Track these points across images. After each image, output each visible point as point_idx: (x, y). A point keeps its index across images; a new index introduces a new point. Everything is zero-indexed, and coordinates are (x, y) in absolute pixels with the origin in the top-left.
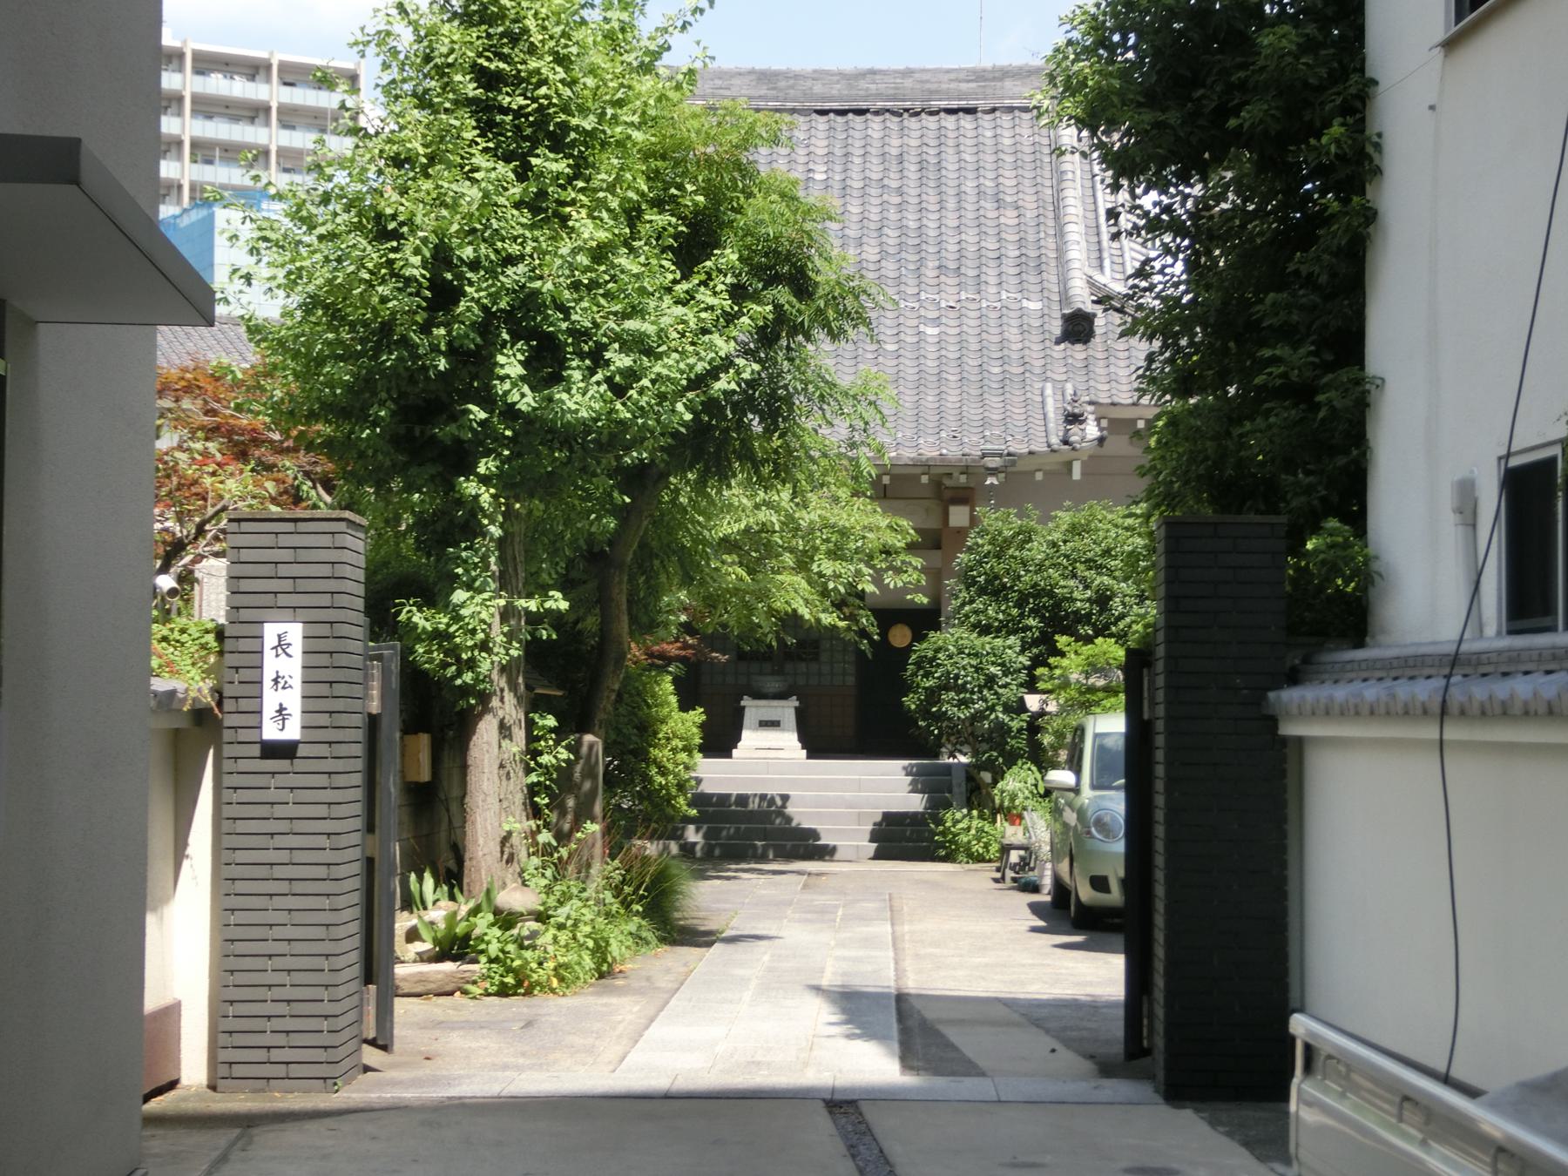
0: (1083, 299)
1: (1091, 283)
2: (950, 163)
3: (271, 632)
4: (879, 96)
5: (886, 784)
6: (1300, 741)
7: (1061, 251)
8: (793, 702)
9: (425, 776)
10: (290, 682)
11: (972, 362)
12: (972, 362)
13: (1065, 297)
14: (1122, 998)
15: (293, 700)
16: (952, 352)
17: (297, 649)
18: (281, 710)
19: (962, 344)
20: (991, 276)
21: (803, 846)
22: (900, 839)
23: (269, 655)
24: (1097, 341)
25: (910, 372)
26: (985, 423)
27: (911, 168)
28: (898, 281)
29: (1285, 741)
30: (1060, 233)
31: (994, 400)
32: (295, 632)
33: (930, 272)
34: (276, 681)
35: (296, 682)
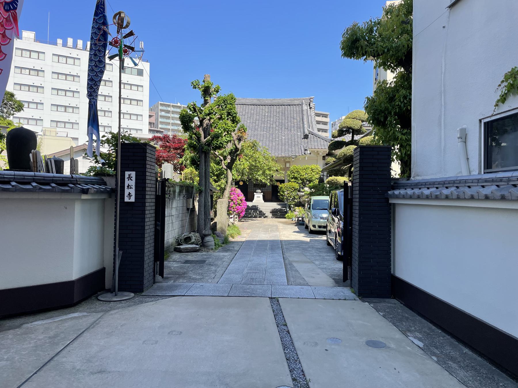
0: (307, 132)
3: (127, 173)
5: (275, 205)
6: (394, 204)
7: (303, 126)
8: (262, 194)
11: (290, 142)
12: (290, 142)
13: (304, 132)
14: (26, 40)
15: (133, 191)
17: (134, 178)
18: (129, 194)
19: (288, 139)
20: (293, 129)
21: (262, 215)
23: (126, 180)
25: (280, 144)
28: (279, 130)
29: (391, 204)
30: (303, 123)
31: (293, 148)
32: (133, 174)
34: (128, 187)
35: (134, 187)
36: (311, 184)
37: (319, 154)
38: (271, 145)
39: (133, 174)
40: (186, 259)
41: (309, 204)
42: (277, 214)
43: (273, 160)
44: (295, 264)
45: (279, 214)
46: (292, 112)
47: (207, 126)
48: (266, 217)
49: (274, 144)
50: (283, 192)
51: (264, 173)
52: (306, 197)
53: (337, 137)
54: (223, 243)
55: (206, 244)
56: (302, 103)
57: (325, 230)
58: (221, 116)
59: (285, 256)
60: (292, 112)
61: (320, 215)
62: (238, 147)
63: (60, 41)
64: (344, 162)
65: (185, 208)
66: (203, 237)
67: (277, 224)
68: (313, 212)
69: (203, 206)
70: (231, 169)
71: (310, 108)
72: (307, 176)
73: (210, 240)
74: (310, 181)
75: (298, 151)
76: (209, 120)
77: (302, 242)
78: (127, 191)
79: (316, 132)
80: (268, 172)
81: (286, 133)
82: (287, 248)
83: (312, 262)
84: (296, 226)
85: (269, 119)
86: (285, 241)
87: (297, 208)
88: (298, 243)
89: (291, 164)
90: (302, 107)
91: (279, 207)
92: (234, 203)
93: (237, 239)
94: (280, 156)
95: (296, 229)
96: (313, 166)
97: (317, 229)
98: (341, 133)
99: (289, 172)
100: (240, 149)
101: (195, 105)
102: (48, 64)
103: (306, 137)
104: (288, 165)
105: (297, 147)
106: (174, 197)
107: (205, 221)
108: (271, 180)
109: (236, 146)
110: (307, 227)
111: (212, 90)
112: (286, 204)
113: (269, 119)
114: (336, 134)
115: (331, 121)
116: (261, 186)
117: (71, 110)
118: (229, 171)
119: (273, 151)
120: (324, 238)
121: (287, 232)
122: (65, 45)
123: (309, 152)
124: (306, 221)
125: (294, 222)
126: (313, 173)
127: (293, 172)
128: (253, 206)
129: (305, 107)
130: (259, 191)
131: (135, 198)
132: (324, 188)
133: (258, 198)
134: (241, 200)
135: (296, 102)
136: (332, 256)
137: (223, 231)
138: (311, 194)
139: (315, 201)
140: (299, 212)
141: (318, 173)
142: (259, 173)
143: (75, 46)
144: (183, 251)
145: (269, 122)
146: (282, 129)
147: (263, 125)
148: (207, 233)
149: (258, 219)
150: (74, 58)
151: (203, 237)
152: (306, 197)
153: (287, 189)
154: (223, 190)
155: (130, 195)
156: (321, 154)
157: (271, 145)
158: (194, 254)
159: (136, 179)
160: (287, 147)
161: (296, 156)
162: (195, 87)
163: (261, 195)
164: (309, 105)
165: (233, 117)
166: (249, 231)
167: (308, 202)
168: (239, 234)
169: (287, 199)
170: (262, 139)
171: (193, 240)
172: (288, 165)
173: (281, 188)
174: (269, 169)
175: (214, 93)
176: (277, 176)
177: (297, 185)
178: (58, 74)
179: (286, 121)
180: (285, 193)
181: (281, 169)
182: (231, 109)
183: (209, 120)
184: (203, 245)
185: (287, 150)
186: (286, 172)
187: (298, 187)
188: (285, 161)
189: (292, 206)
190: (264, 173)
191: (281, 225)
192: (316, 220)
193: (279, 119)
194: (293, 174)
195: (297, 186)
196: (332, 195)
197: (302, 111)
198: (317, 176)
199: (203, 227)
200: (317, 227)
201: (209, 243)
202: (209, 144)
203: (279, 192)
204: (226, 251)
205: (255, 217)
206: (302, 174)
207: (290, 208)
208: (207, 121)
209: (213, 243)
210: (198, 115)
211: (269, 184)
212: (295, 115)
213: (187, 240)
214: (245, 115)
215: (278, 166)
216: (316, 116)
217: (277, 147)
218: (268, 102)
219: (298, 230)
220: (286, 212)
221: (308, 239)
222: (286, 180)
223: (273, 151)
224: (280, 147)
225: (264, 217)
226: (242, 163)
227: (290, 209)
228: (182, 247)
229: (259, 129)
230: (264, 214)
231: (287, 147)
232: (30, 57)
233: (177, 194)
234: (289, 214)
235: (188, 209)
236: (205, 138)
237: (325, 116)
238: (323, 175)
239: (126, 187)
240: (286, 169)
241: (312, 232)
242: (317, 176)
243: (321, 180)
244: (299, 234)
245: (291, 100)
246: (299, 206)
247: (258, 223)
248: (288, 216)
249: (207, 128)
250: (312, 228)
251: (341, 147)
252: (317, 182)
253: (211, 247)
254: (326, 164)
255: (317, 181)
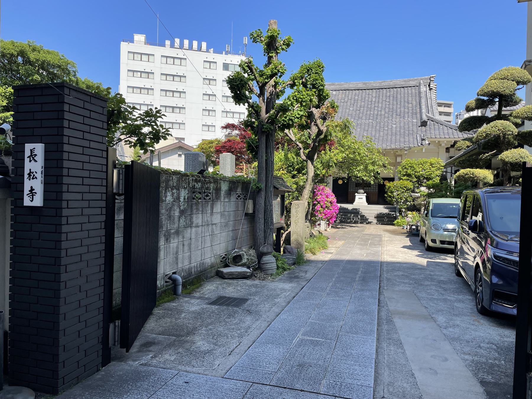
0: (425, 118)
1: (427, 116)
2: (399, 96)
3: (28, 147)
4: (386, 86)
5: (381, 209)
9: (251, 211)
10: (36, 175)
11: (402, 131)
12: (402, 131)
13: (421, 118)
15: (38, 185)
16: (398, 129)
18: (32, 189)
20: (406, 115)
21: (364, 220)
22: (381, 219)
23: (27, 160)
24: (428, 126)
25: (390, 133)
26: (405, 142)
27: (391, 98)
28: (388, 117)
30: (420, 107)
31: (407, 138)
32: (39, 148)
33: (394, 116)
34: (29, 175)
35: (39, 176)
36: (430, 182)
37: (441, 145)
38: (378, 135)
39: (39, 148)
40: (222, 293)
41: (427, 209)
42: (384, 220)
43: (379, 152)
44: (398, 322)
45: (386, 219)
46: (406, 95)
47: (271, 95)
48: (369, 223)
49: (382, 133)
50: (392, 192)
51: (366, 168)
52: (422, 199)
53: (473, 110)
54: (294, 264)
55: (264, 266)
56: (420, 84)
57: (453, 247)
58: (294, 82)
59: (382, 298)
60: (406, 95)
61: (444, 226)
62: (322, 128)
63: (168, 43)
64: (484, 149)
65: (240, 212)
66: (260, 255)
67: (382, 233)
68: (433, 220)
69: (263, 211)
70: (312, 160)
71: (430, 89)
72: (424, 172)
73: (270, 260)
74: (428, 179)
75: (413, 142)
76: (275, 86)
77: (413, 267)
78: (28, 184)
79: (438, 117)
80: (371, 167)
81: (398, 120)
82: (388, 280)
83: (430, 318)
84: (407, 237)
85: (376, 105)
86: (388, 263)
87: (410, 212)
88: (409, 268)
89: (403, 157)
90: (420, 89)
91: (386, 211)
92: (322, 207)
93: (322, 256)
94: (388, 148)
95: (407, 242)
96: (433, 160)
97: (438, 245)
98: (481, 104)
99: (400, 168)
100: (324, 131)
101: (250, 63)
102: (157, 66)
103: (424, 124)
104: (399, 159)
105: (411, 137)
106: (218, 197)
107: (265, 232)
108: (376, 178)
109: (318, 128)
110: (423, 241)
111: (280, 42)
112: (395, 208)
113: (376, 105)
114: (473, 105)
115: (455, 111)
116: (363, 185)
117: (177, 110)
118: (309, 162)
119: (381, 143)
120: (450, 259)
121: (393, 248)
122: (172, 46)
123: (427, 142)
124: (423, 230)
125: (405, 231)
126: (433, 169)
127: (406, 168)
128: (354, 209)
129: (423, 89)
130: (362, 191)
131: (45, 200)
132: (448, 186)
133: (360, 200)
134: (331, 202)
135: (412, 83)
136: (465, 303)
137: (299, 245)
138: (430, 196)
139: (435, 205)
140: (412, 218)
141: (439, 169)
142: (358, 169)
143: (181, 47)
144: (226, 276)
145: (376, 108)
146: (392, 116)
147: (368, 113)
148: (265, 250)
149: (359, 225)
150: (181, 59)
151: (260, 255)
152: (422, 199)
153: (397, 189)
154: (300, 190)
155: (34, 192)
156: (443, 145)
157: (378, 135)
158: (241, 282)
159: (46, 160)
160: (398, 137)
161: (410, 148)
162: (255, 41)
163: (364, 197)
164: (429, 86)
165: (320, 91)
166: (340, 243)
167: (425, 205)
168: (325, 247)
169: (397, 202)
170: (367, 128)
171: (244, 261)
172: (399, 159)
173: (390, 187)
174: (373, 163)
175: (284, 47)
176: (385, 173)
177: (411, 183)
178: (167, 75)
179: (399, 106)
180: (395, 194)
181: (390, 164)
182: (317, 80)
183: (275, 86)
184: (258, 268)
185: (398, 141)
186: (396, 168)
187: (412, 187)
188: (396, 154)
189: (404, 210)
190: (366, 168)
191: (387, 235)
192: (437, 232)
193: (389, 105)
194: (405, 170)
195: (410, 185)
196: (466, 197)
197: (420, 93)
198: (438, 172)
199: (262, 241)
200: (438, 242)
201: (268, 266)
202: (273, 121)
203: (386, 193)
204: (292, 278)
205: (356, 222)
206: (418, 170)
207: (400, 212)
208: (271, 88)
209: (274, 265)
210: (255, 78)
211: (372, 182)
212: (410, 99)
213: (237, 260)
214: (347, 102)
215: (385, 160)
216: (439, 106)
217: (385, 137)
218: (376, 84)
219: (409, 244)
220: (396, 218)
221: (423, 261)
222: (396, 178)
223: (381, 143)
224: (389, 137)
225: (367, 224)
226: (334, 155)
227: (401, 214)
228: (226, 270)
229: (364, 118)
230: (367, 219)
231: (398, 137)
232: (141, 60)
233: (223, 193)
234: (399, 220)
235: (247, 214)
236: (267, 113)
237: (448, 106)
238: (446, 172)
239: (26, 176)
240: (396, 164)
241: (430, 249)
242: (439, 173)
243: (443, 178)
244: (410, 251)
245: (405, 81)
246: (412, 210)
247: (357, 231)
248: (398, 222)
249: (271, 99)
250: (431, 244)
251: (480, 126)
252: (437, 180)
253: (270, 272)
254: (451, 157)
255: (438, 178)
